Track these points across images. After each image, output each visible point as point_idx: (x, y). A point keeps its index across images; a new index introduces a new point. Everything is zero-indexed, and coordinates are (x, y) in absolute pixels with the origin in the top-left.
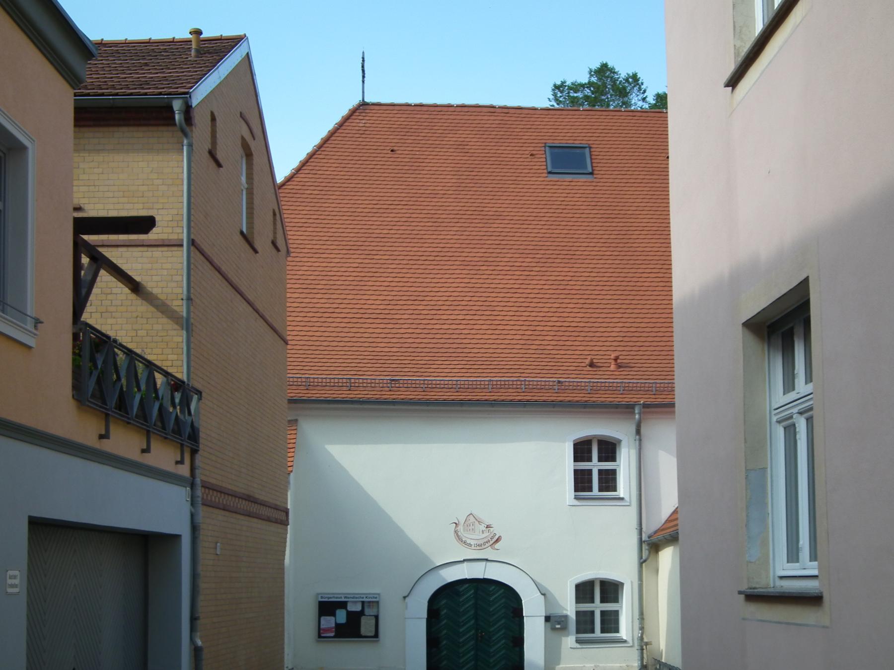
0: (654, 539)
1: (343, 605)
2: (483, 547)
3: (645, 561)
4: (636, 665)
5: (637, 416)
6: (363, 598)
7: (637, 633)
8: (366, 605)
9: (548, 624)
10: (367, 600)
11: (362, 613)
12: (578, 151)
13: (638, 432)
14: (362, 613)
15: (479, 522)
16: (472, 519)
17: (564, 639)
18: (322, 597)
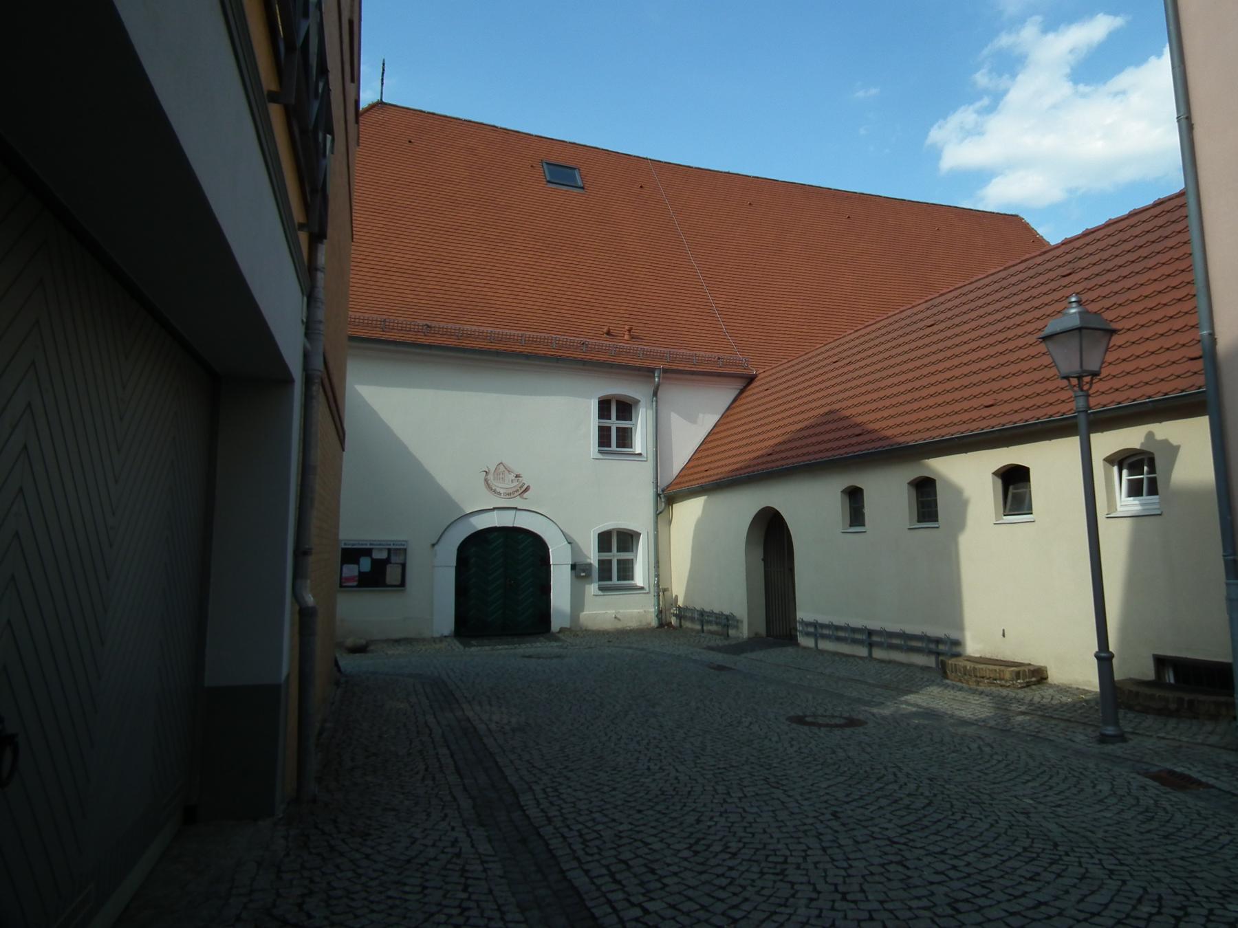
0: (670, 491)
1: (367, 552)
2: (512, 496)
3: (661, 513)
4: (653, 610)
5: (657, 379)
6: (390, 545)
7: (653, 581)
8: (392, 552)
9: (573, 572)
10: (394, 547)
11: (387, 561)
12: (569, 171)
13: (655, 394)
14: (387, 561)
15: (509, 471)
16: (501, 466)
17: (587, 586)
18: (345, 544)
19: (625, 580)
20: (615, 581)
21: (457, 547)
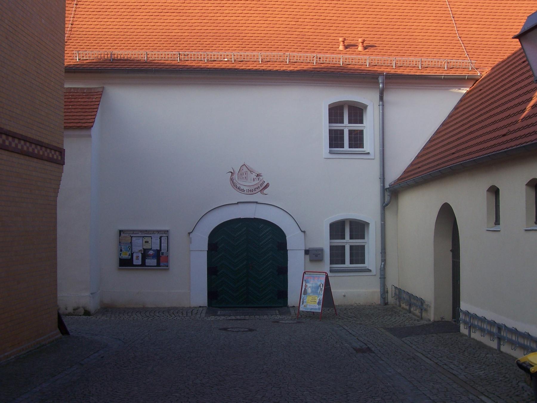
2: (254, 192)
5: (381, 86)
15: (251, 171)
16: (244, 167)
19: (357, 263)
20: (347, 264)
21: (209, 234)
